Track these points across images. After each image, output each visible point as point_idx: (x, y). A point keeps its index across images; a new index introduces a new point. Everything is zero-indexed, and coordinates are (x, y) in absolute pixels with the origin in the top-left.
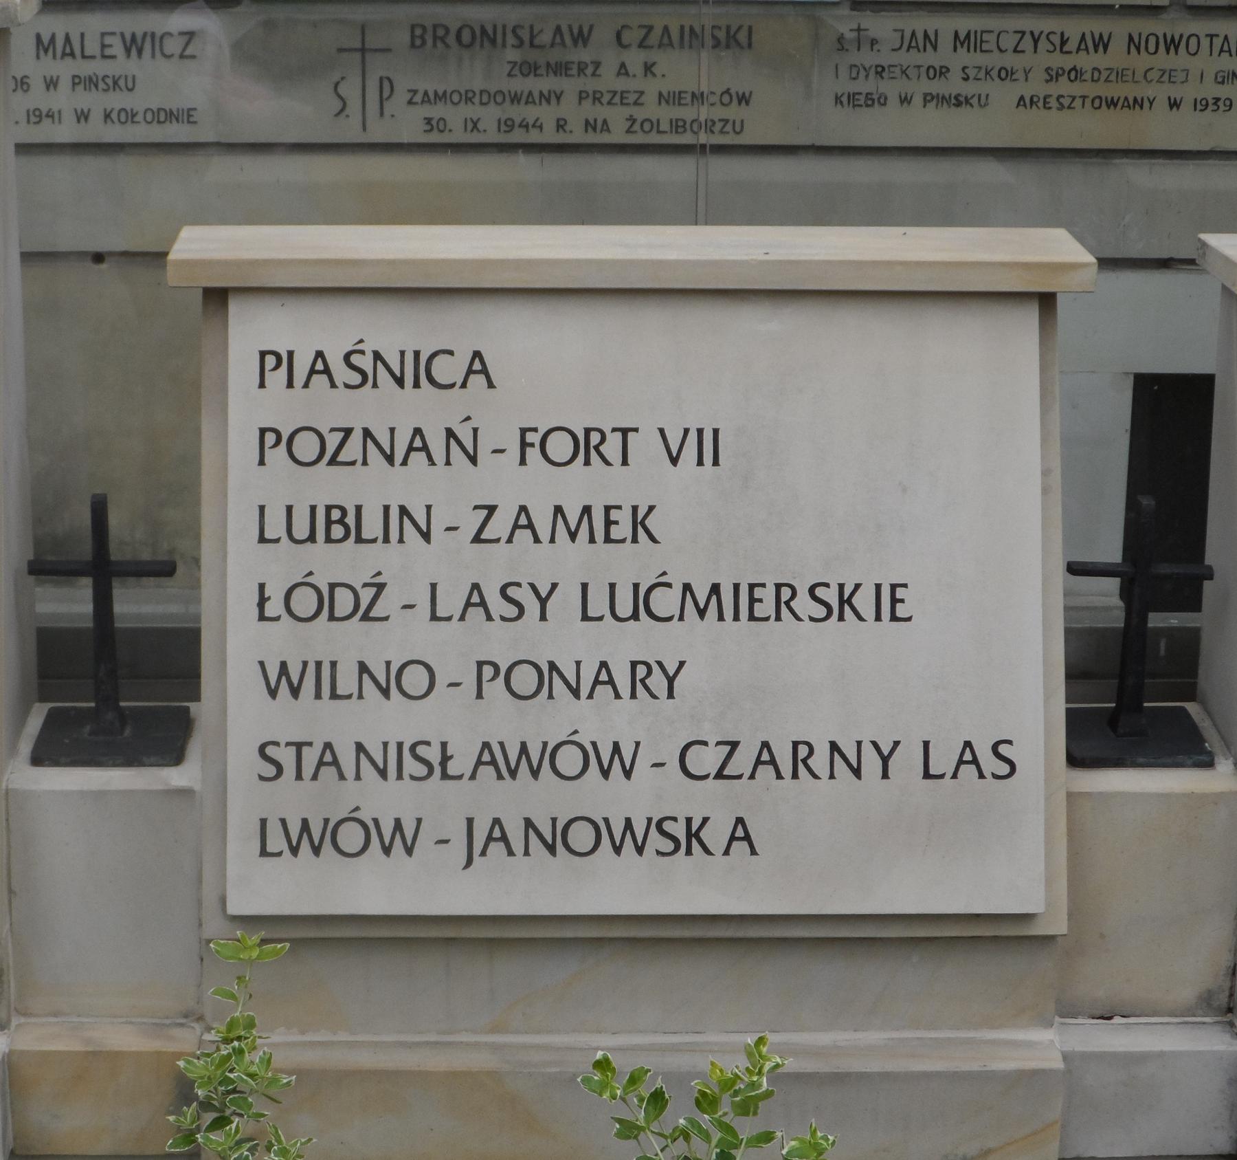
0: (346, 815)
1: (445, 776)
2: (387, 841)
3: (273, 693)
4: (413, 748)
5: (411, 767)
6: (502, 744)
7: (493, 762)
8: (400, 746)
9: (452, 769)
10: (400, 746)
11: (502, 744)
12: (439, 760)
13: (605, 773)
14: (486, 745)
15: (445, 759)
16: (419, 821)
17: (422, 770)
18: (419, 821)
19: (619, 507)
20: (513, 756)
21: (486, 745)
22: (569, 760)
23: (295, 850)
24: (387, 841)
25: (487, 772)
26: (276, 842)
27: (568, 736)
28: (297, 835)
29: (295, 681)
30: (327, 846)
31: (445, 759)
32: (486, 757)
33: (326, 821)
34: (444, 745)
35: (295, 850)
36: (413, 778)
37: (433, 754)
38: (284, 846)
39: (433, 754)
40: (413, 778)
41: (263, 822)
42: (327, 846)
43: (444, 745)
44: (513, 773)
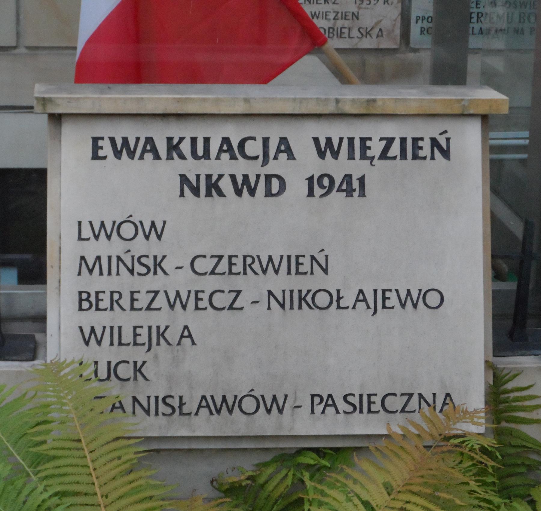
0: (125, 219)
1: (181, 414)
2: (147, 232)
3: (87, 343)
4: (164, 399)
5: (162, 408)
6: (212, 397)
7: (208, 406)
8: (157, 398)
9: (185, 410)
10: (157, 398)
11: (212, 397)
12: (178, 405)
13: (269, 411)
14: (204, 397)
15: (181, 404)
16: (165, 222)
17: (169, 411)
18: (165, 222)
19: (304, 256)
20: (219, 402)
21: (204, 397)
22: (249, 405)
23: (97, 237)
24: (147, 232)
25: (204, 412)
26: (87, 232)
27: (249, 392)
28: (99, 228)
29: (99, 337)
30: (115, 235)
31: (181, 404)
32: (204, 403)
33: (114, 222)
34: (181, 398)
35: (97, 237)
36: (164, 414)
37: (176, 403)
38: (91, 235)
39: (176, 403)
40: (164, 414)
41: (80, 223)
42: (115, 235)
43: (181, 398)
44: (219, 411)
